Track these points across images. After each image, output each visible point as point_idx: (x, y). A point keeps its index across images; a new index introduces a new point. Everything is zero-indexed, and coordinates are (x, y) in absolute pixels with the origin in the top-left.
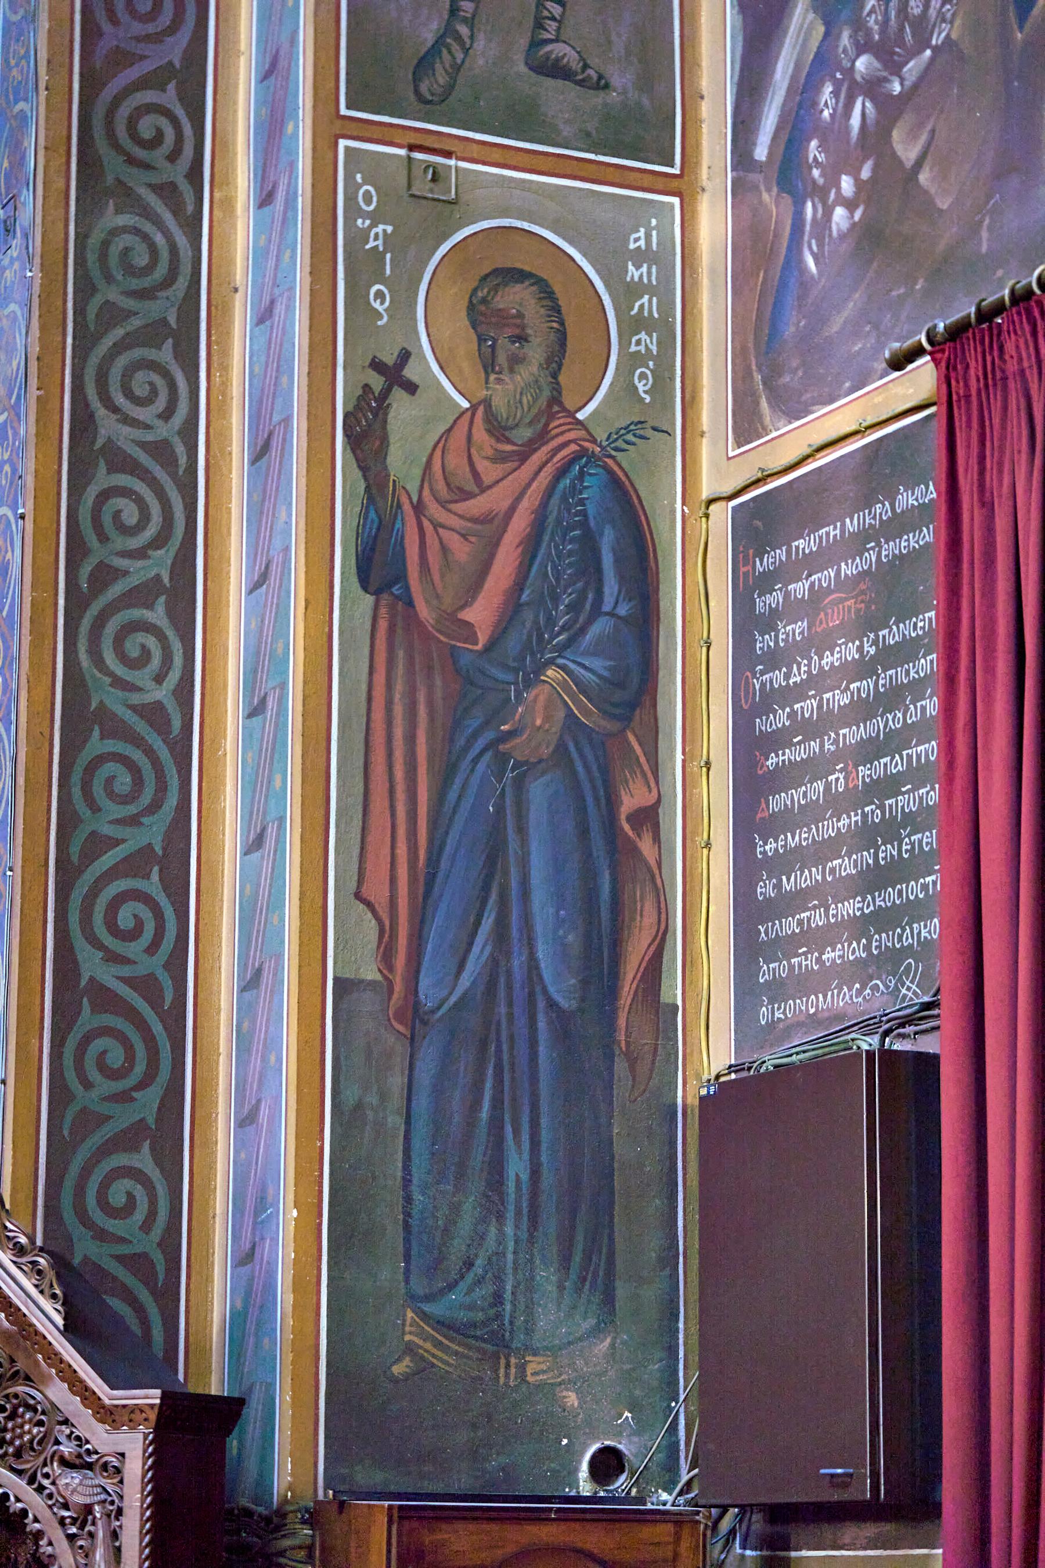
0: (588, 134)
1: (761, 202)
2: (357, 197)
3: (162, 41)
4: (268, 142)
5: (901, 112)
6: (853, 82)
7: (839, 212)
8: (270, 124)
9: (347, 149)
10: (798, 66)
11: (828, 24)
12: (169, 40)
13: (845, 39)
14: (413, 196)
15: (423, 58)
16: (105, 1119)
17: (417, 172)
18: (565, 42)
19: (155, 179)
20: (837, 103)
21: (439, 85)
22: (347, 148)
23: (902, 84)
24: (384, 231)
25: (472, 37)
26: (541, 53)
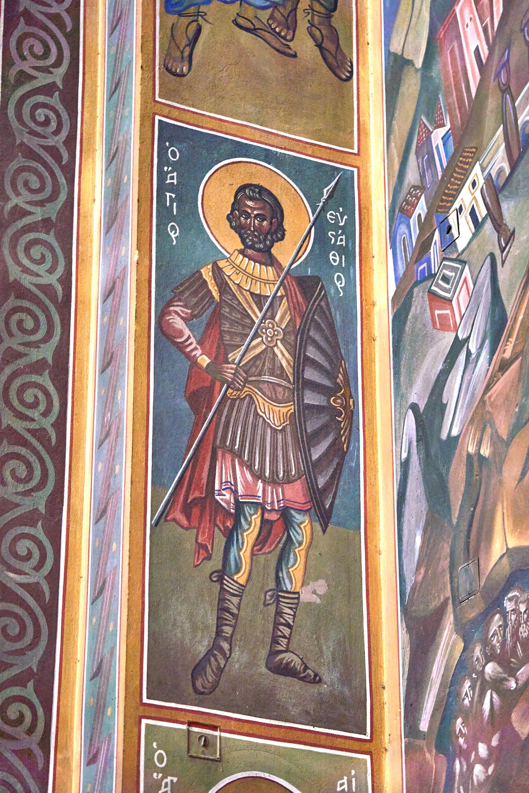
0: (308, 713)
1: (425, 759)
2: (153, 758)
3: (25, 654)
4: (94, 720)
5: (517, 702)
6: (484, 681)
7: (478, 769)
8: (96, 709)
9: (147, 725)
10: (447, 669)
11: (465, 641)
12: (29, 653)
13: (478, 652)
14: (191, 757)
15: (198, 665)
16: (27, 213)
17: (194, 740)
18: (292, 652)
19: (17, 746)
20: (474, 694)
21: (209, 682)
23: (517, 683)
24: (172, 781)
25: (230, 650)
26: (277, 659)
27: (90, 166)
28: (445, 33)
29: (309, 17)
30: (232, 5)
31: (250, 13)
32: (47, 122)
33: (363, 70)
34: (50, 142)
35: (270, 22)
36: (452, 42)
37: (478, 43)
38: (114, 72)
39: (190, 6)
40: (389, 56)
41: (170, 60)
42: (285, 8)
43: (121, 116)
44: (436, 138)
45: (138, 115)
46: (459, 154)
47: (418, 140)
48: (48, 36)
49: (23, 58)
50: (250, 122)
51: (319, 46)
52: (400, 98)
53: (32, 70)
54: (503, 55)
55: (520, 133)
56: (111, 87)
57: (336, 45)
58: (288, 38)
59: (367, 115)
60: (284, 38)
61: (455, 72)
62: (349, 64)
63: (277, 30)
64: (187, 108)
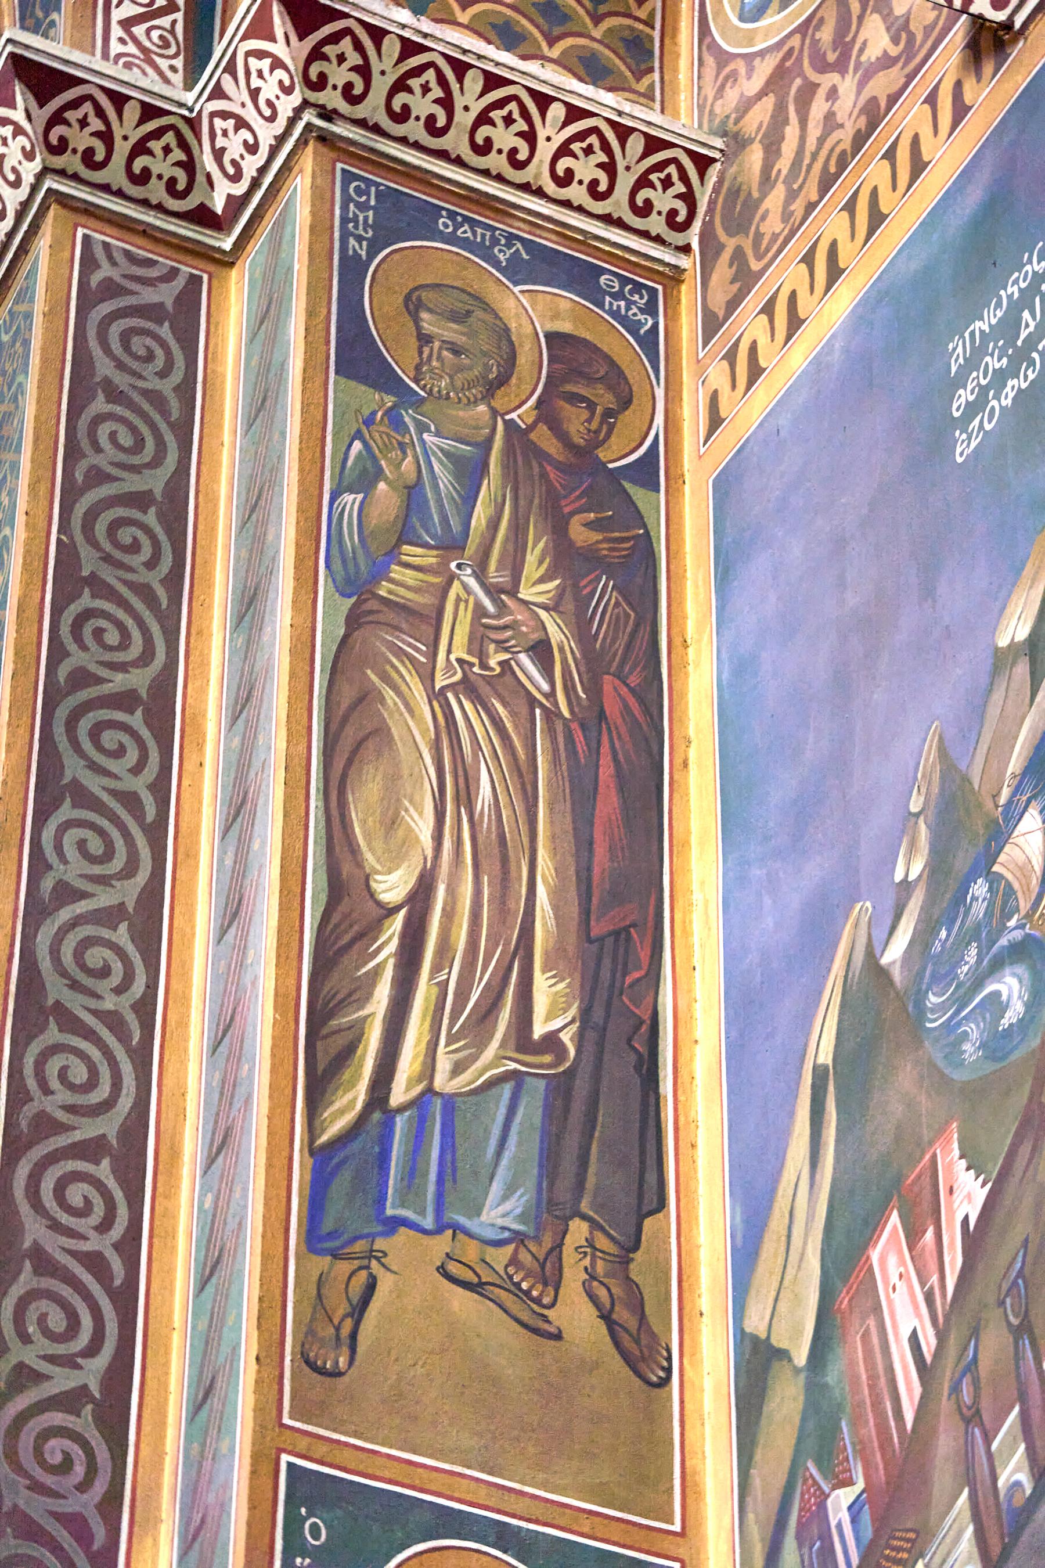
22: (290, 1465)
27: (148, 1555)
28: (850, 1301)
29: (587, 1262)
30: (438, 1237)
31: (471, 1251)
32: (66, 1465)
33: (691, 1364)
34: (68, 1506)
35: (511, 1270)
36: (863, 1319)
37: (916, 1323)
38: (202, 1366)
39: (356, 1239)
40: (742, 1341)
41: (312, 1344)
42: (540, 1245)
43: (214, 1455)
44: (837, 1510)
45: (247, 1453)
46: (883, 1542)
47: (801, 1510)
48: (76, 1296)
49: (25, 1339)
50: (469, 1467)
51: (606, 1317)
52: (764, 1421)
53: (42, 1362)
54: (965, 1348)
55: (1004, 1507)
56: (197, 1395)
57: (638, 1317)
58: (546, 1300)
59: (700, 1456)
60: (538, 1301)
61: (873, 1378)
62: (665, 1354)
63: (525, 1286)
64: (343, 1438)
